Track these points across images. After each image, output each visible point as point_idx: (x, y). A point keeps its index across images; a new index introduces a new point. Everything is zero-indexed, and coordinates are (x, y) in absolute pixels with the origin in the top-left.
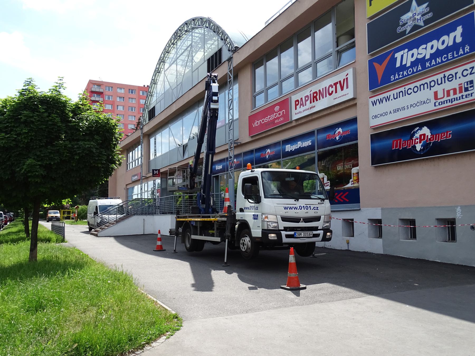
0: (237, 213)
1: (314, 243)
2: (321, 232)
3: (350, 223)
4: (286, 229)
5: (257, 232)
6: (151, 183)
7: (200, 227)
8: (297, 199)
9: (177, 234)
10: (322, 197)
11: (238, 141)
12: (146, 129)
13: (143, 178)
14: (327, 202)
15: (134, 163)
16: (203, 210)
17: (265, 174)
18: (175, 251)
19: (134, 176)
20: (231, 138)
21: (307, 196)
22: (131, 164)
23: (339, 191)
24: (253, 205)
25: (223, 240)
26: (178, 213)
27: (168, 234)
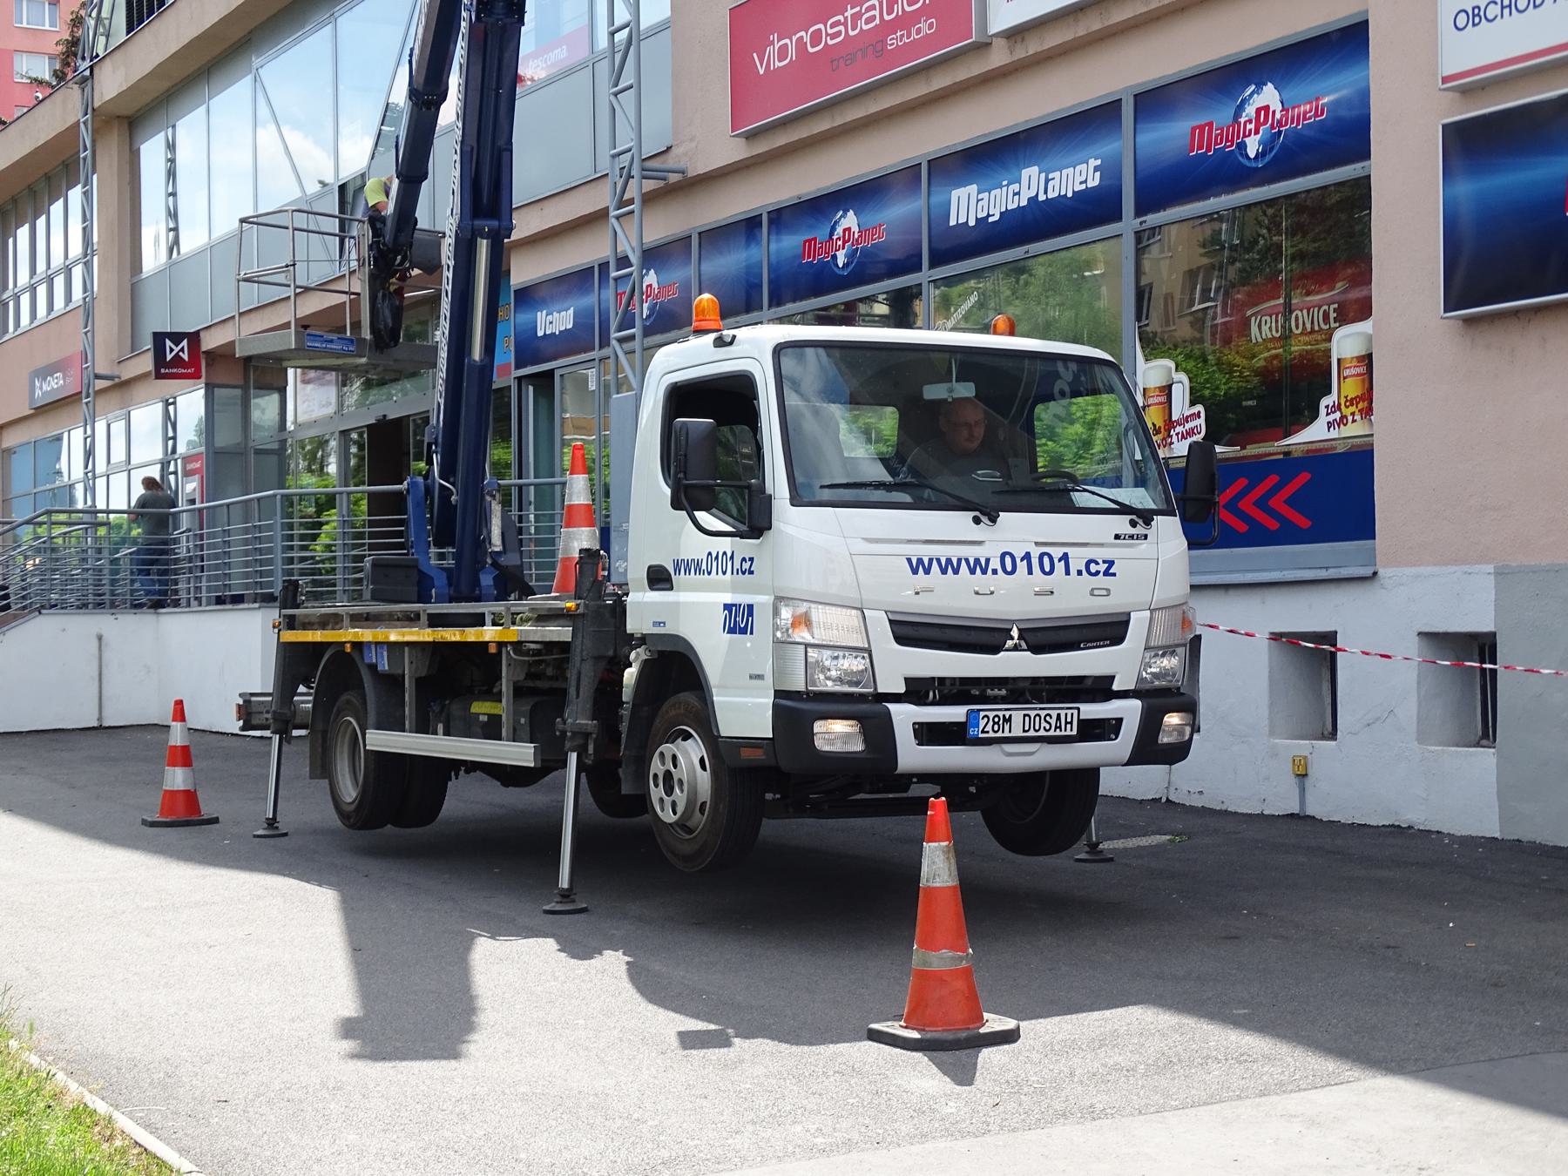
0: (629, 599)
1: (1090, 775)
2: (1130, 711)
3: (1315, 656)
4: (917, 691)
5: (744, 712)
6: (147, 417)
7: (420, 683)
8: (987, 512)
9: (284, 723)
10: (1139, 498)
11: (670, 162)
12: (111, 84)
13: (100, 384)
14: (1169, 529)
15: (42, 291)
16: (440, 580)
17: (801, 359)
18: (272, 823)
19: (45, 372)
20: (625, 140)
21: (1053, 496)
22: (25, 300)
23: (1260, 467)
24: (725, 544)
25: (550, 763)
26: (290, 596)
27: (234, 726)
